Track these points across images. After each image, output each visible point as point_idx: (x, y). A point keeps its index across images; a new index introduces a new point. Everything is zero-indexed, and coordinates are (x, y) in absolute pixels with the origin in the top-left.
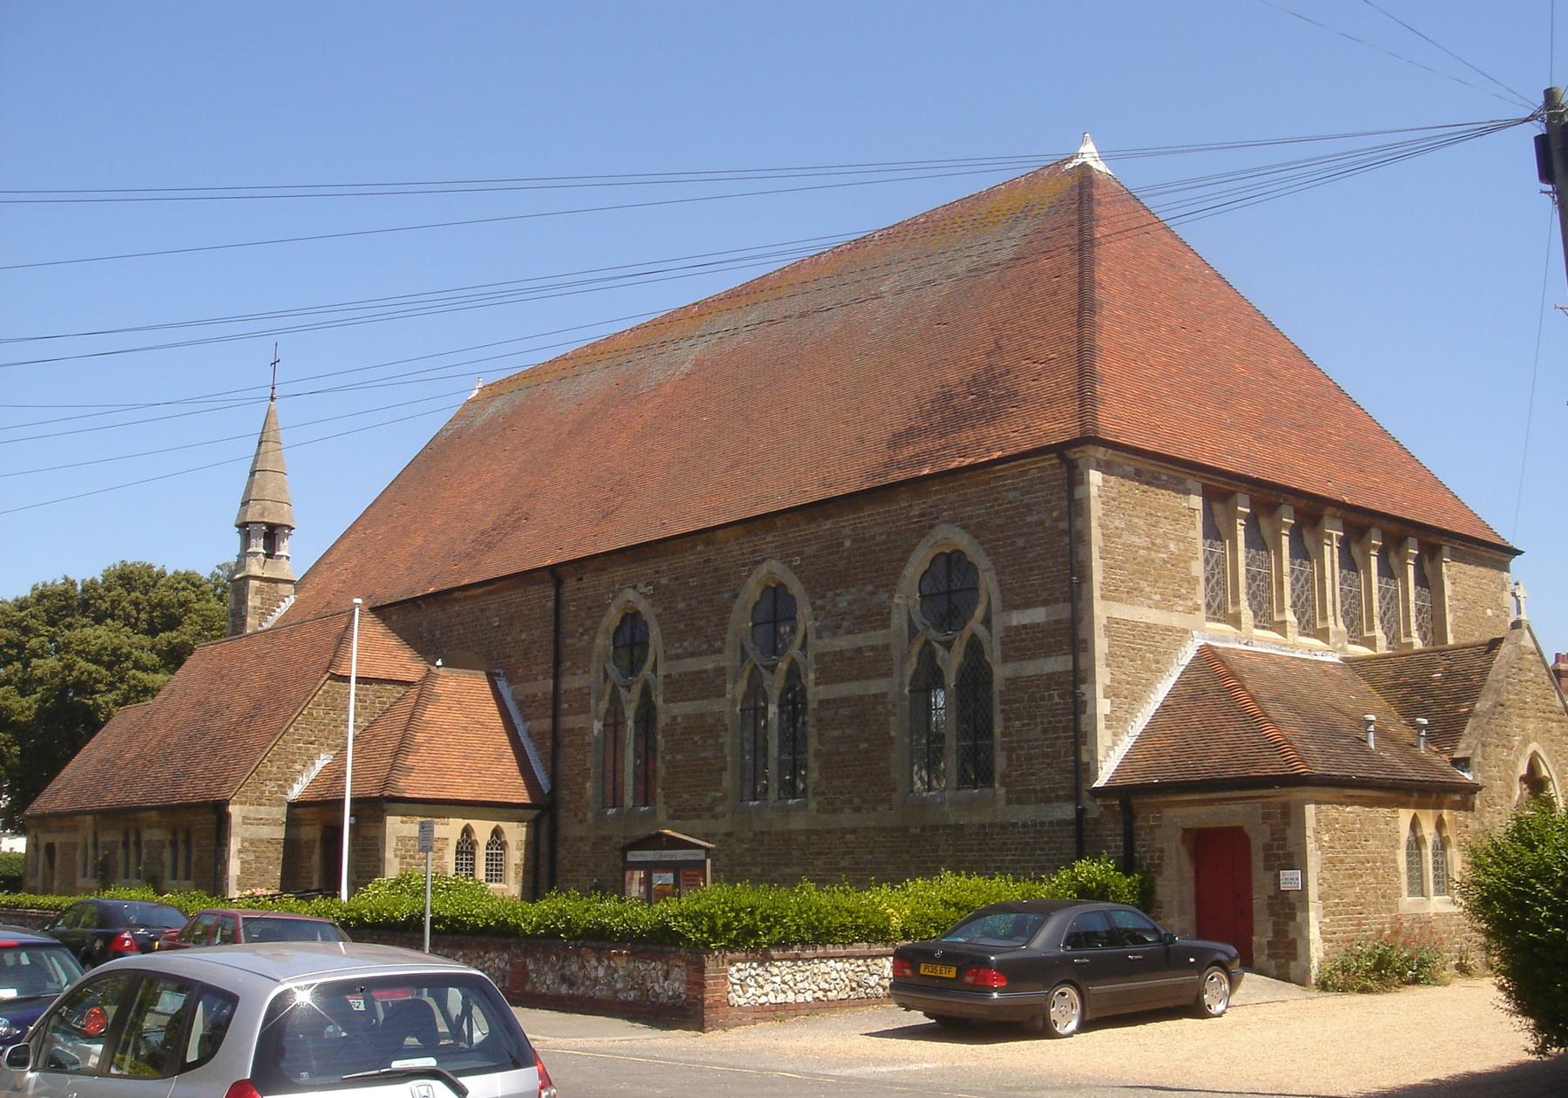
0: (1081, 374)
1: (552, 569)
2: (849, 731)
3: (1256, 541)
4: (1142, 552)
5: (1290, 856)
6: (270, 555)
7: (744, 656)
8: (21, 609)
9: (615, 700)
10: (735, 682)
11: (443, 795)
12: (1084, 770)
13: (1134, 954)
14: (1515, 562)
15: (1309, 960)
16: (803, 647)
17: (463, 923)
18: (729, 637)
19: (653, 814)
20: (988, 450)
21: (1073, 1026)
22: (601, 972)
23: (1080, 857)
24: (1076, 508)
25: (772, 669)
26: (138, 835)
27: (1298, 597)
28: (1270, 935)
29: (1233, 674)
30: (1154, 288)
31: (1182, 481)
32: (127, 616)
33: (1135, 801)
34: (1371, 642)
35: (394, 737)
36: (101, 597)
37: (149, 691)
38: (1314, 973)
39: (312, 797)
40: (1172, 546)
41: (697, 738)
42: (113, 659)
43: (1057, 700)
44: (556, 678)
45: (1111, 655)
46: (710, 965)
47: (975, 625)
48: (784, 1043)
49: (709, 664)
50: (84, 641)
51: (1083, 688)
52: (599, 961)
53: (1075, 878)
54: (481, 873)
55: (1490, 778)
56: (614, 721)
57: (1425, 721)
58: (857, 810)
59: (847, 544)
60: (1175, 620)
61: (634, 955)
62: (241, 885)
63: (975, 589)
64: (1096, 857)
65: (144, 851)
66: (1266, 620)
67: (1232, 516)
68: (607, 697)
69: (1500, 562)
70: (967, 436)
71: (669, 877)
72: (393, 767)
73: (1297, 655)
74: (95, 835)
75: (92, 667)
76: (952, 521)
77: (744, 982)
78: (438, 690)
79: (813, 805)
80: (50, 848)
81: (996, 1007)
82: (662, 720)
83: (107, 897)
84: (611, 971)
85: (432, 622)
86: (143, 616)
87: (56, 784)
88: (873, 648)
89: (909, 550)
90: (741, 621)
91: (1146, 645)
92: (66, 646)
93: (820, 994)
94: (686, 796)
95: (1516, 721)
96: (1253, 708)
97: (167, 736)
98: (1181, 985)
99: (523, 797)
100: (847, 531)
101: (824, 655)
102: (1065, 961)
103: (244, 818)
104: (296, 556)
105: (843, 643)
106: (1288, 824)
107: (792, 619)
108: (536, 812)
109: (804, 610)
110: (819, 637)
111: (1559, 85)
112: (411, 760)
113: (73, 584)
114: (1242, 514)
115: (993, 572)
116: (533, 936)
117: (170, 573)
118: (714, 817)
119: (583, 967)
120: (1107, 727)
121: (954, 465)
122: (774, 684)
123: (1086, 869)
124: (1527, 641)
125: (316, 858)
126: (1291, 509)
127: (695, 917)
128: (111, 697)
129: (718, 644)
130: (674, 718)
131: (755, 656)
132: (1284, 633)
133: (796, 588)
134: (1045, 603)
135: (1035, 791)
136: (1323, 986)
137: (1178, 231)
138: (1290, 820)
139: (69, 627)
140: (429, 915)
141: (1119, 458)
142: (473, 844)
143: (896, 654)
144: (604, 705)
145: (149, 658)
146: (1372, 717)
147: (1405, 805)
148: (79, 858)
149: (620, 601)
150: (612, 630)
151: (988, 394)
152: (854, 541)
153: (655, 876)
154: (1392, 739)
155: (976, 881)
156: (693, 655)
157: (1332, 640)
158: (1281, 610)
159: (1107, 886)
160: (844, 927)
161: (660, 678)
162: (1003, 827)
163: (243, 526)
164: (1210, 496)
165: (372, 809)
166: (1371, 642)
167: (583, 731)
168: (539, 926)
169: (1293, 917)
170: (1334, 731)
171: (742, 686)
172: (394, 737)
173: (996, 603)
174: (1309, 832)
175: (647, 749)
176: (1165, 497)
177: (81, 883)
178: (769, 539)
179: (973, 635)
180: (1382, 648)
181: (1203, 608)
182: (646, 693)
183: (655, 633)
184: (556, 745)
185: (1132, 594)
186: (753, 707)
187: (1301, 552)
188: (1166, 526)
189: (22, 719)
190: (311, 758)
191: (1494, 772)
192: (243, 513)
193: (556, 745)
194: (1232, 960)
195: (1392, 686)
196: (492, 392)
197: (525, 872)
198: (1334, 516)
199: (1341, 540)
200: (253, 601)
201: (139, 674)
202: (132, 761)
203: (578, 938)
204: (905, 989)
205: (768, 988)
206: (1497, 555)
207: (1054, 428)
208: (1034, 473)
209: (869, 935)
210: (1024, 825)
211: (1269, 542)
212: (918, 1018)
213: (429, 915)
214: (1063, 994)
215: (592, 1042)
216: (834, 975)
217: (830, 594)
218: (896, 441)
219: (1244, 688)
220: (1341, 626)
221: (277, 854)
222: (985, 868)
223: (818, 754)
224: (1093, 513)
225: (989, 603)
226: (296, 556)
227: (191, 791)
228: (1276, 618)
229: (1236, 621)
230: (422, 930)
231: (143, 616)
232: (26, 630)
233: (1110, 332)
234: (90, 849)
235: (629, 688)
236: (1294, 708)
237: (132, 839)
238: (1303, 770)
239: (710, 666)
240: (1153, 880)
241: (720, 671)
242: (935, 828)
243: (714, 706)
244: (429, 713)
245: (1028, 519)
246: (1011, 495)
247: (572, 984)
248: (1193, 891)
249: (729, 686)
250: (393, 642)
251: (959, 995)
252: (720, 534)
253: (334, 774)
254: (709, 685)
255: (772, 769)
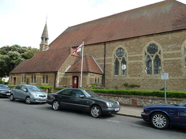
7: (146, 54)
13: (60, 96)
49: (138, 55)
59: (170, 38)
74: (25, 76)
88: (177, 53)
104: (49, 42)
177: (21, 83)
184: (105, 66)
193: (105, 66)
200: (44, 47)
237: (34, 77)
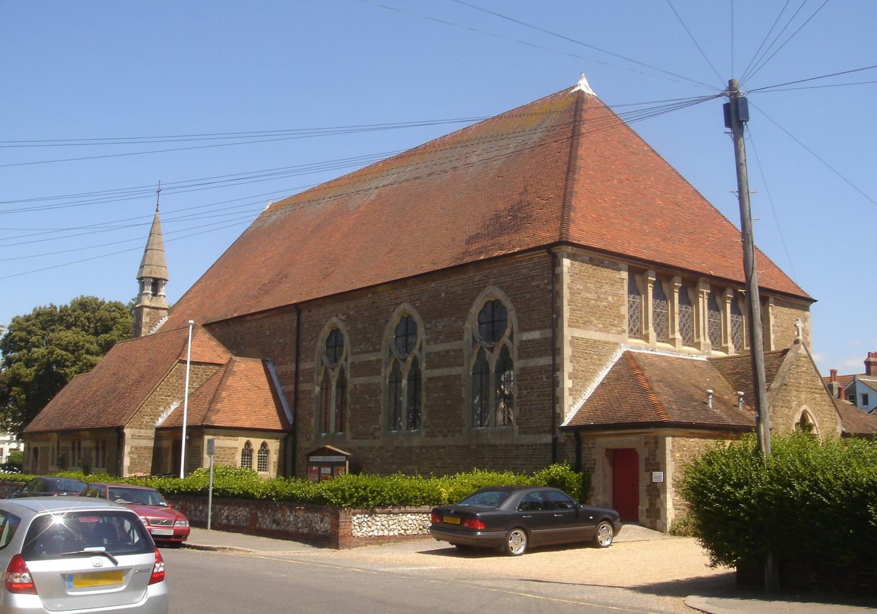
0: (564, 206)
1: (296, 305)
2: (442, 394)
3: (660, 295)
4: (592, 302)
5: (658, 464)
6: (155, 294)
8: (27, 321)
9: (326, 374)
10: (386, 367)
11: (235, 425)
12: (557, 417)
14: (812, 306)
15: (666, 519)
16: (420, 349)
17: (228, 492)
18: (384, 343)
19: (344, 437)
20: (514, 247)
21: (521, 550)
22: (292, 518)
23: (554, 462)
24: (556, 278)
25: (404, 360)
26: (79, 444)
27: (684, 325)
28: (647, 506)
29: (638, 367)
30: (613, 158)
31: (616, 264)
32: (83, 326)
33: (582, 434)
34: (726, 350)
35: (209, 394)
36: (70, 315)
37: (92, 366)
38: (669, 526)
39: (167, 425)
40: (610, 299)
41: (366, 397)
42: (75, 348)
43: (545, 380)
44: (297, 363)
45: (573, 356)
46: (342, 515)
47: (505, 339)
48: (384, 556)
50: (60, 339)
51: (558, 373)
52: (291, 512)
53: (549, 474)
54: (255, 466)
55: (777, 424)
56: (326, 388)
57: (742, 393)
58: (445, 436)
59: (443, 295)
60: (611, 338)
61: (307, 510)
62: (130, 471)
63: (506, 320)
64: (561, 463)
65: (82, 452)
66: (664, 335)
67: (645, 282)
68: (322, 374)
69: (803, 306)
70: (505, 239)
71: (328, 470)
72: (209, 410)
73: (681, 356)
74: (58, 444)
75: (64, 353)
76: (495, 284)
77: (360, 525)
78: (235, 369)
79: (423, 433)
80: (36, 450)
81: (479, 539)
82: (350, 386)
83: (48, 477)
84: (292, 518)
85: (235, 333)
86: (92, 325)
87: (39, 416)
88: (454, 351)
89: (473, 299)
90: (389, 335)
91: (593, 352)
92: (50, 342)
93: (402, 532)
94: (361, 427)
95: (794, 393)
96: (646, 386)
97: (96, 391)
98: (586, 530)
99: (278, 426)
100: (443, 288)
101: (430, 353)
102: (517, 517)
103: (132, 435)
104: (169, 295)
105: (440, 347)
106: (657, 448)
107: (415, 334)
108: (286, 434)
109: (421, 330)
110: (428, 344)
111: (737, 80)
112: (219, 406)
113: (55, 308)
114: (651, 282)
115: (514, 312)
116: (260, 499)
117: (107, 302)
118: (375, 438)
119: (283, 516)
120: (570, 395)
121: (496, 254)
122: (406, 369)
123: (556, 470)
124: (802, 351)
125: (170, 457)
126: (680, 279)
127: (334, 491)
128: (74, 369)
129: (378, 347)
130: (355, 386)
131: (396, 353)
132: (674, 345)
133: (417, 318)
134: (540, 328)
135: (533, 428)
136: (673, 533)
137: (632, 126)
138: (657, 446)
139: (53, 331)
140: (211, 488)
141: (580, 252)
142: (251, 451)
143: (466, 354)
144: (321, 378)
145: (94, 348)
146: (711, 391)
147: (727, 438)
148: (50, 454)
149: (329, 323)
150: (394, 327)
151: (517, 217)
152: (446, 294)
153: (322, 469)
154: (724, 403)
155: (493, 475)
156: (366, 352)
157: (702, 348)
158: (673, 332)
159: (565, 478)
160: (416, 497)
161: (349, 365)
162: (517, 447)
163: (141, 279)
164: (632, 272)
165: (197, 431)
166: (726, 350)
167: (310, 392)
168: (263, 494)
169: (659, 496)
170: (691, 398)
171: (390, 369)
172: (209, 394)
173: (516, 329)
174: (668, 452)
175: (342, 405)
176: (606, 273)
177: (51, 468)
178: (404, 291)
179: (504, 345)
180: (732, 352)
181: (627, 332)
182: (342, 372)
183: (347, 340)
184: (297, 399)
185: (586, 324)
186: (396, 378)
187: (685, 300)
188: (606, 288)
189: (27, 380)
190: (168, 404)
191: (780, 421)
192: (141, 272)
193: (297, 399)
194: (615, 518)
195: (732, 374)
196: (275, 208)
197: (279, 466)
198: (705, 282)
199: (709, 295)
200: (145, 319)
201: (89, 357)
202: (78, 404)
203: (281, 501)
204: (438, 529)
205: (373, 528)
206: (803, 302)
207: (546, 236)
208: (536, 260)
209: (430, 501)
210: (528, 445)
211: (667, 296)
212: (446, 545)
213: (211, 488)
214: (517, 534)
215: (279, 553)
216: (410, 522)
217: (434, 321)
218: (469, 242)
219: (643, 375)
220: (708, 341)
221: (149, 455)
222: (499, 468)
223: (426, 406)
224: (565, 282)
225: (512, 330)
226: (169, 295)
227: (106, 421)
228: (671, 337)
229: (646, 338)
230: (208, 496)
231: (92, 325)
232: (30, 332)
233: (583, 183)
234: (56, 451)
235: (333, 369)
236: (670, 386)
237: (76, 446)
238: (665, 419)
239: (374, 358)
240: (590, 476)
241: (379, 361)
242: (483, 446)
243: (376, 379)
244: (230, 381)
245: (533, 284)
246: (524, 271)
247: (278, 524)
248: (611, 482)
249: (383, 370)
250: (214, 343)
251: (466, 532)
252: (380, 289)
253: (179, 413)
254: (372, 368)
255: (404, 412)
